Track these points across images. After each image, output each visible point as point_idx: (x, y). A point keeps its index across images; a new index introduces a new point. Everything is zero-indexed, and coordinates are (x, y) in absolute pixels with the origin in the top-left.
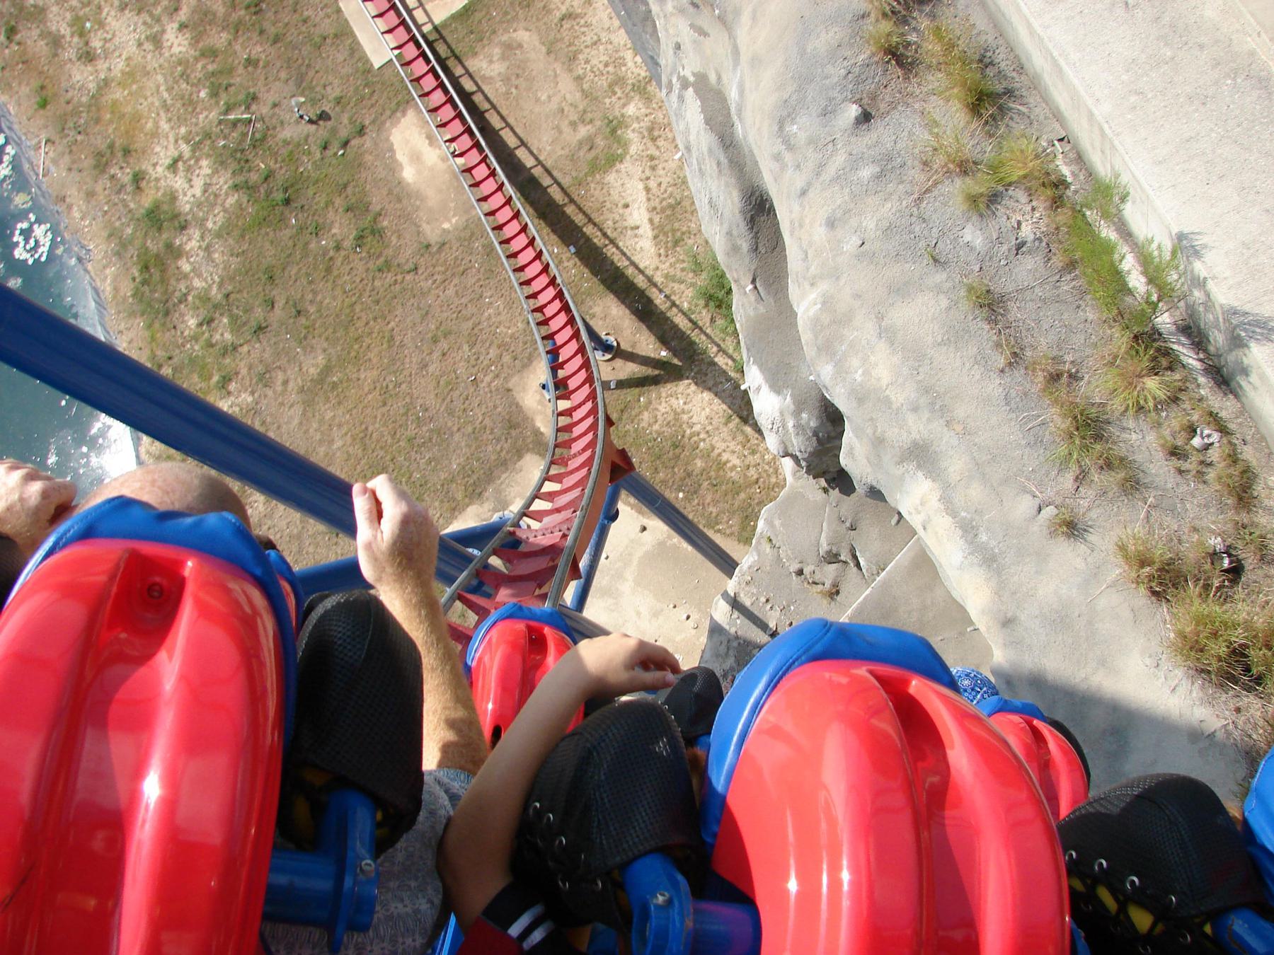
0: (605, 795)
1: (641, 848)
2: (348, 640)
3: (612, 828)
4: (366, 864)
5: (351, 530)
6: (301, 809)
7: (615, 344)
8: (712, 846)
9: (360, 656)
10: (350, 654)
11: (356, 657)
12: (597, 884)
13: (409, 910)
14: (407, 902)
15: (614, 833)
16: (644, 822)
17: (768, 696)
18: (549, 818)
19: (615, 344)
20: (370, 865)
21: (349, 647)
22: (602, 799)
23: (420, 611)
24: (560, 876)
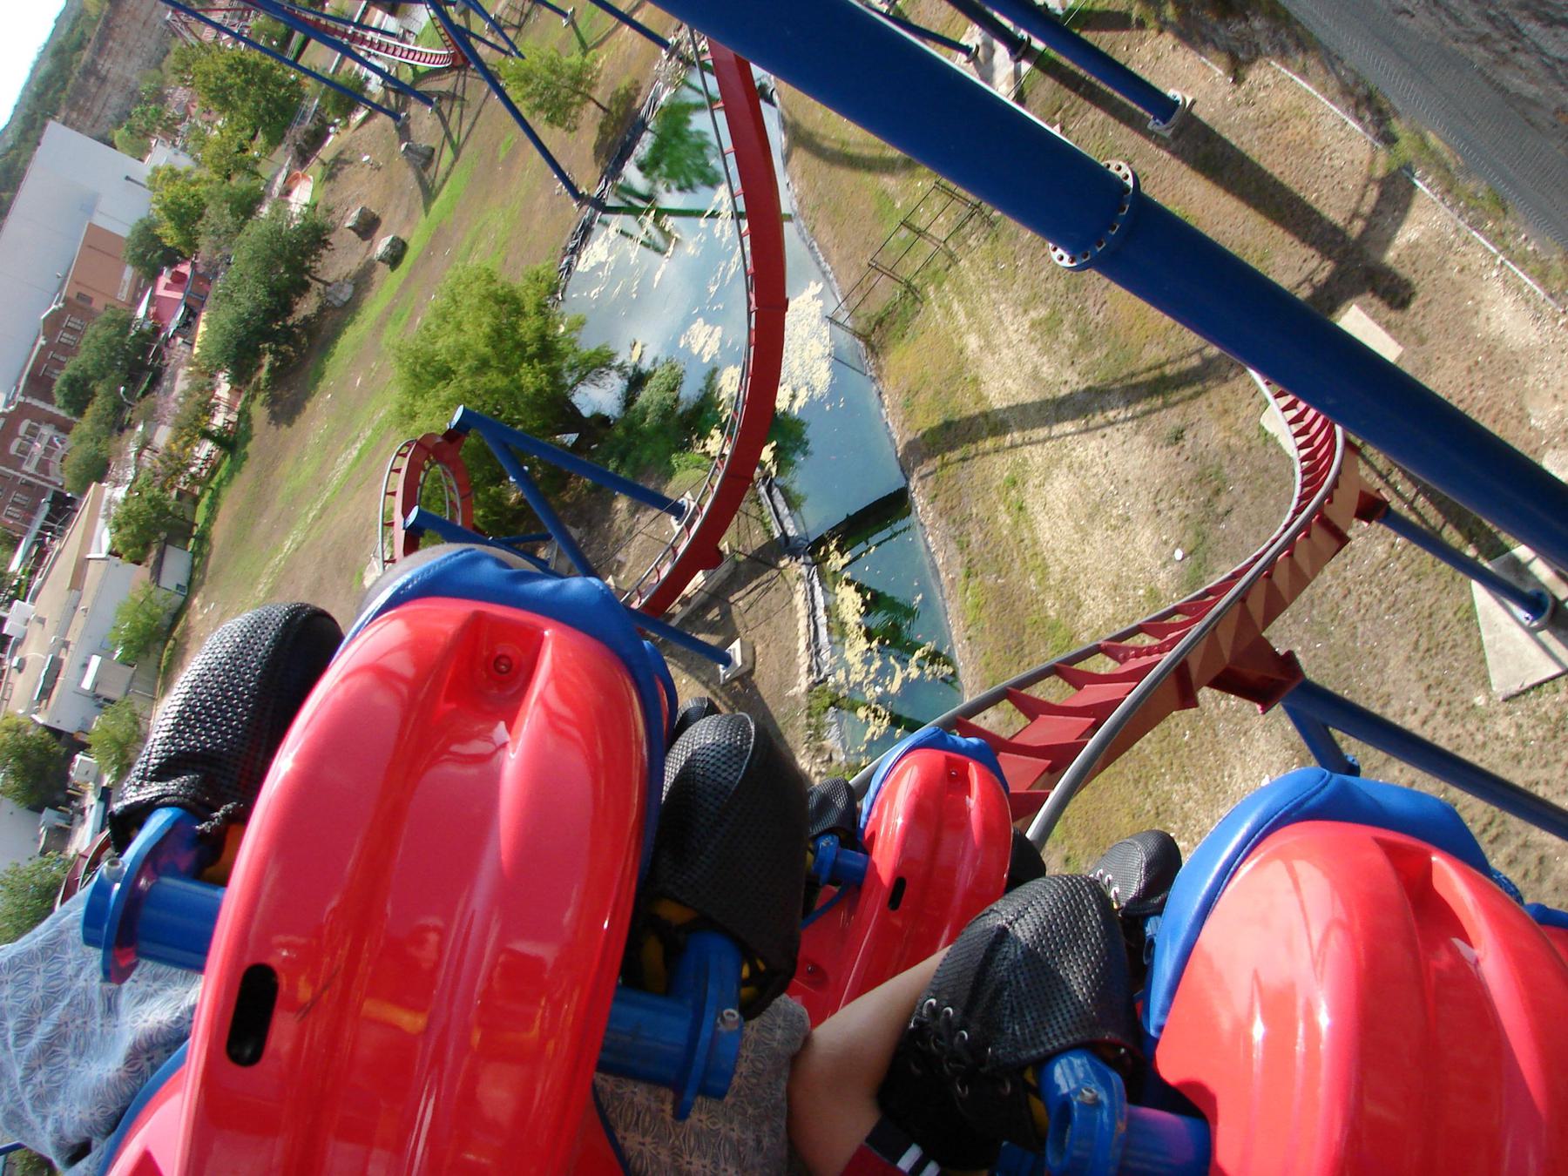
0: (1021, 978)
1: (1063, 1041)
2: (723, 759)
3: (1028, 1018)
4: (729, 1014)
5: (80, 413)
6: (653, 951)
7: (1130, 182)
8: (1156, 1041)
9: (736, 778)
10: (724, 775)
11: (731, 778)
12: (1004, 1087)
13: (734, 1135)
14: (736, 1126)
15: (1030, 1023)
16: (1069, 1012)
17: (1246, 857)
18: (948, 1013)
19: (1130, 182)
20: (733, 1015)
21: (724, 767)
22: (1018, 982)
23: (443, 761)
24: (958, 1079)
